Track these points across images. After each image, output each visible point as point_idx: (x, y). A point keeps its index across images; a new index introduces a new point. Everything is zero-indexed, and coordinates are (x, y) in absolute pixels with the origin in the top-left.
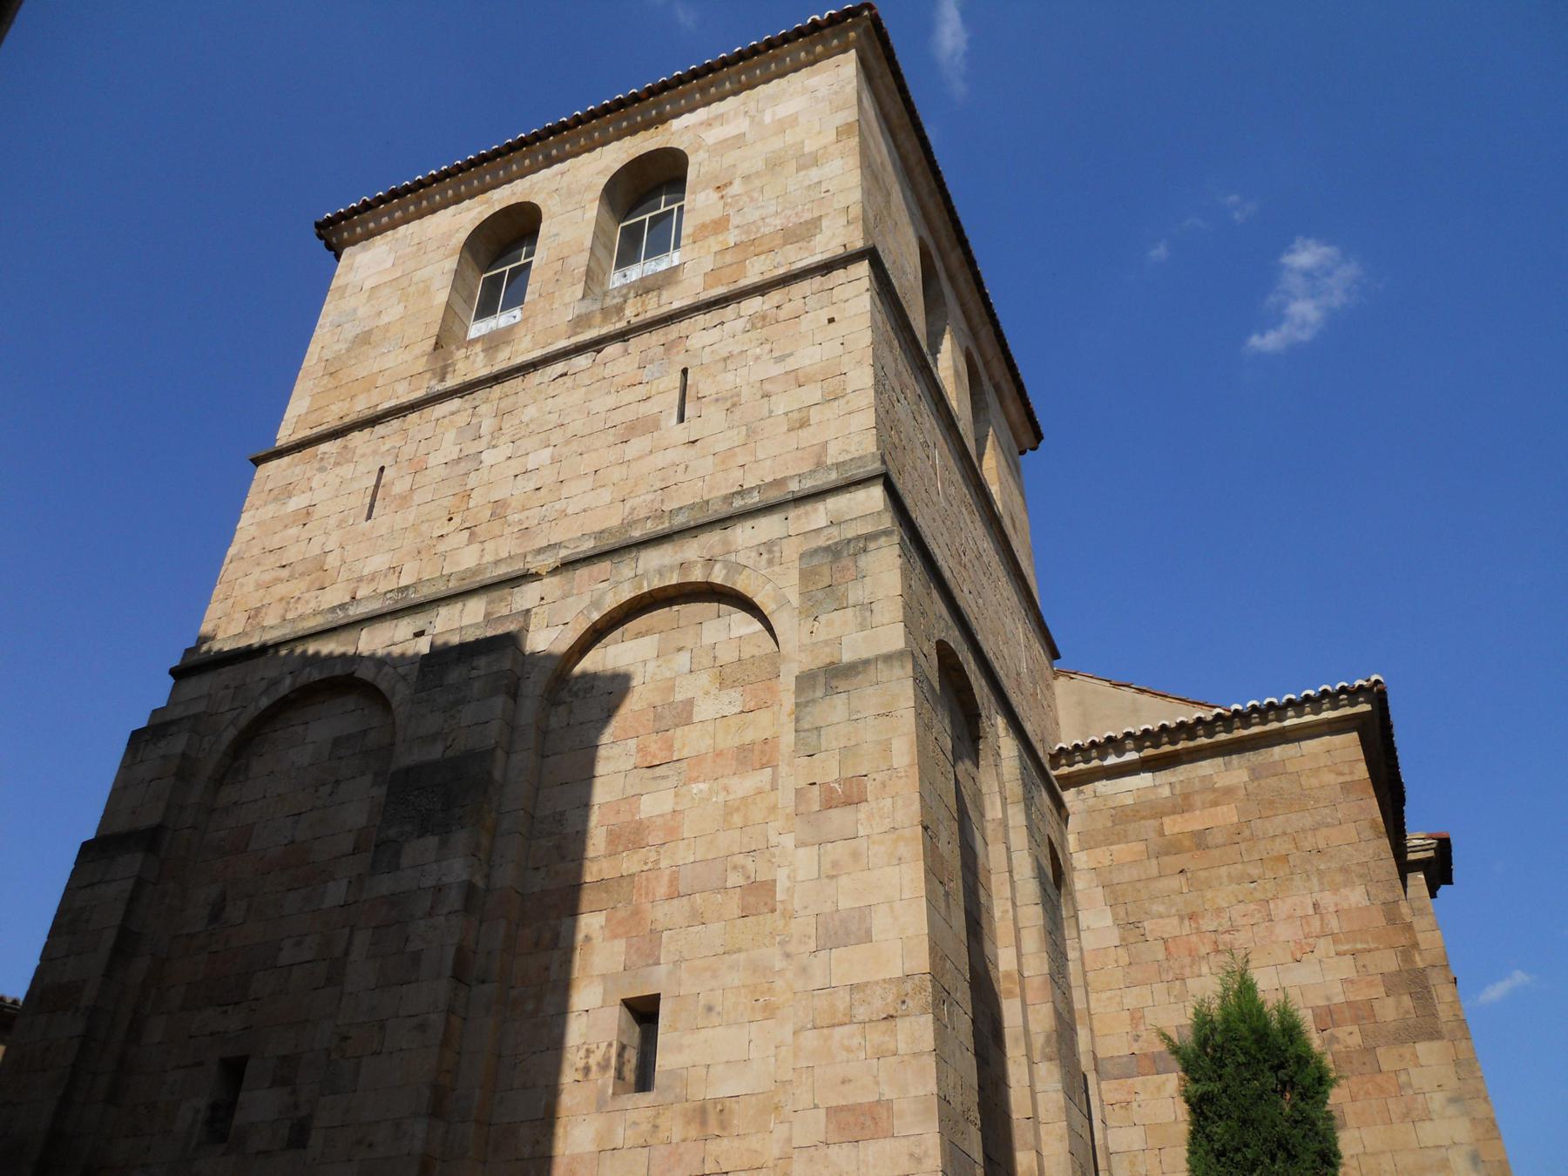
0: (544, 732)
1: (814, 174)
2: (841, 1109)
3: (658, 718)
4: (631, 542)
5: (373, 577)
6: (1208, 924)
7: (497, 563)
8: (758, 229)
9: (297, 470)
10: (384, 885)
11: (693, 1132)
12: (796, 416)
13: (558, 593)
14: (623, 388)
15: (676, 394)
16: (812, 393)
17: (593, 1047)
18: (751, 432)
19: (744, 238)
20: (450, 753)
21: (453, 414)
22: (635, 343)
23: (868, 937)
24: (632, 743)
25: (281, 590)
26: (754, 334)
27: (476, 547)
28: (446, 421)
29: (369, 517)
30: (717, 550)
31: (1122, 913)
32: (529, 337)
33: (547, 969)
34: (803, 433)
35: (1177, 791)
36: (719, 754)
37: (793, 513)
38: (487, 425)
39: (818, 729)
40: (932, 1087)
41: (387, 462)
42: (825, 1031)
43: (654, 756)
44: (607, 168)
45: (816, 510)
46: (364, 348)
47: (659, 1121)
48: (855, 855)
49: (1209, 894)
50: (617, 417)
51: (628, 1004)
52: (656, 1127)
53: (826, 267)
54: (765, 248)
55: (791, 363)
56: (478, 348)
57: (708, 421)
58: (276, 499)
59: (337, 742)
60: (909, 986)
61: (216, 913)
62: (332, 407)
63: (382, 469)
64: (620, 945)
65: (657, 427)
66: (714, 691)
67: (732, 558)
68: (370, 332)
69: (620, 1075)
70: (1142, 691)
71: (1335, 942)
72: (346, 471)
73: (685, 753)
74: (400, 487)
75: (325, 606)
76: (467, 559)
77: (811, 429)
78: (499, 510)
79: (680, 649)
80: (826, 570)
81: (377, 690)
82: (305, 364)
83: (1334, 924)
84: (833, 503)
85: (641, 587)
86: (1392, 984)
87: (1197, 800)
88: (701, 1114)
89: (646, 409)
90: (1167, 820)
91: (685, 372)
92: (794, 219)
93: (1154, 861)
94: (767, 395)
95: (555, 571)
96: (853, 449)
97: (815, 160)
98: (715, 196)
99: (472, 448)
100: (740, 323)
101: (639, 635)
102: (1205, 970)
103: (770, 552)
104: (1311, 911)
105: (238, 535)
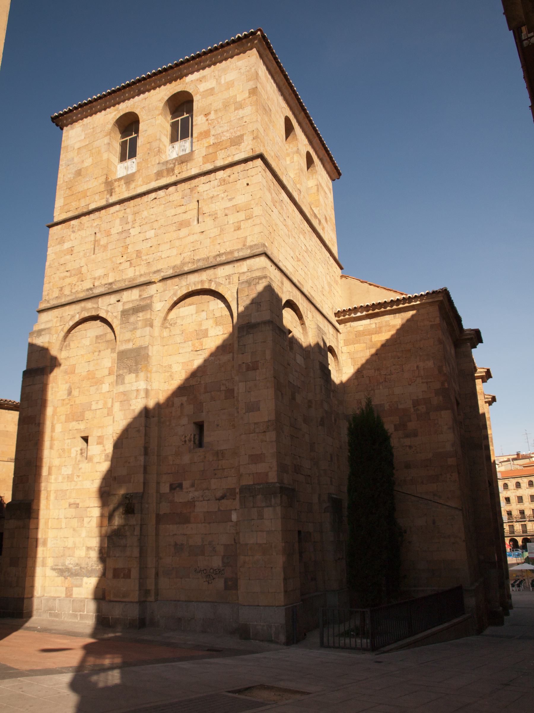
1: (241, 113)
2: (252, 455)
3: (197, 334)
4: (184, 272)
7: (141, 275)
8: (221, 137)
9: (65, 231)
10: (121, 388)
12: (236, 224)
13: (162, 289)
14: (177, 206)
15: (196, 211)
16: (241, 216)
18: (222, 230)
19: (216, 141)
20: (134, 347)
21: (117, 211)
23: (259, 409)
24: (190, 343)
25: (68, 280)
27: (132, 268)
28: (115, 215)
29: (94, 254)
30: (212, 277)
32: (141, 179)
35: (377, 326)
37: (236, 265)
39: (245, 345)
40: (275, 450)
41: (97, 230)
43: (197, 348)
46: (80, 177)
47: (243, 225)
50: (176, 219)
51: (195, 423)
53: (245, 161)
54: (224, 147)
56: (122, 182)
57: (208, 223)
58: (59, 243)
59: (97, 337)
62: (72, 204)
64: (192, 406)
66: (214, 326)
67: (217, 280)
68: (80, 170)
69: (195, 443)
70: (370, 285)
72: (83, 233)
74: (103, 242)
75: (84, 288)
76: (131, 274)
77: (241, 231)
78: (139, 254)
79: (203, 311)
80: (246, 289)
82: (58, 183)
84: (249, 262)
85: (189, 289)
87: (384, 329)
88: (217, 453)
90: (373, 336)
92: (234, 134)
95: (160, 281)
96: (255, 240)
97: (240, 106)
98: (205, 119)
99: (127, 227)
101: (190, 305)
102: (381, 387)
104: (415, 369)
105: (48, 257)
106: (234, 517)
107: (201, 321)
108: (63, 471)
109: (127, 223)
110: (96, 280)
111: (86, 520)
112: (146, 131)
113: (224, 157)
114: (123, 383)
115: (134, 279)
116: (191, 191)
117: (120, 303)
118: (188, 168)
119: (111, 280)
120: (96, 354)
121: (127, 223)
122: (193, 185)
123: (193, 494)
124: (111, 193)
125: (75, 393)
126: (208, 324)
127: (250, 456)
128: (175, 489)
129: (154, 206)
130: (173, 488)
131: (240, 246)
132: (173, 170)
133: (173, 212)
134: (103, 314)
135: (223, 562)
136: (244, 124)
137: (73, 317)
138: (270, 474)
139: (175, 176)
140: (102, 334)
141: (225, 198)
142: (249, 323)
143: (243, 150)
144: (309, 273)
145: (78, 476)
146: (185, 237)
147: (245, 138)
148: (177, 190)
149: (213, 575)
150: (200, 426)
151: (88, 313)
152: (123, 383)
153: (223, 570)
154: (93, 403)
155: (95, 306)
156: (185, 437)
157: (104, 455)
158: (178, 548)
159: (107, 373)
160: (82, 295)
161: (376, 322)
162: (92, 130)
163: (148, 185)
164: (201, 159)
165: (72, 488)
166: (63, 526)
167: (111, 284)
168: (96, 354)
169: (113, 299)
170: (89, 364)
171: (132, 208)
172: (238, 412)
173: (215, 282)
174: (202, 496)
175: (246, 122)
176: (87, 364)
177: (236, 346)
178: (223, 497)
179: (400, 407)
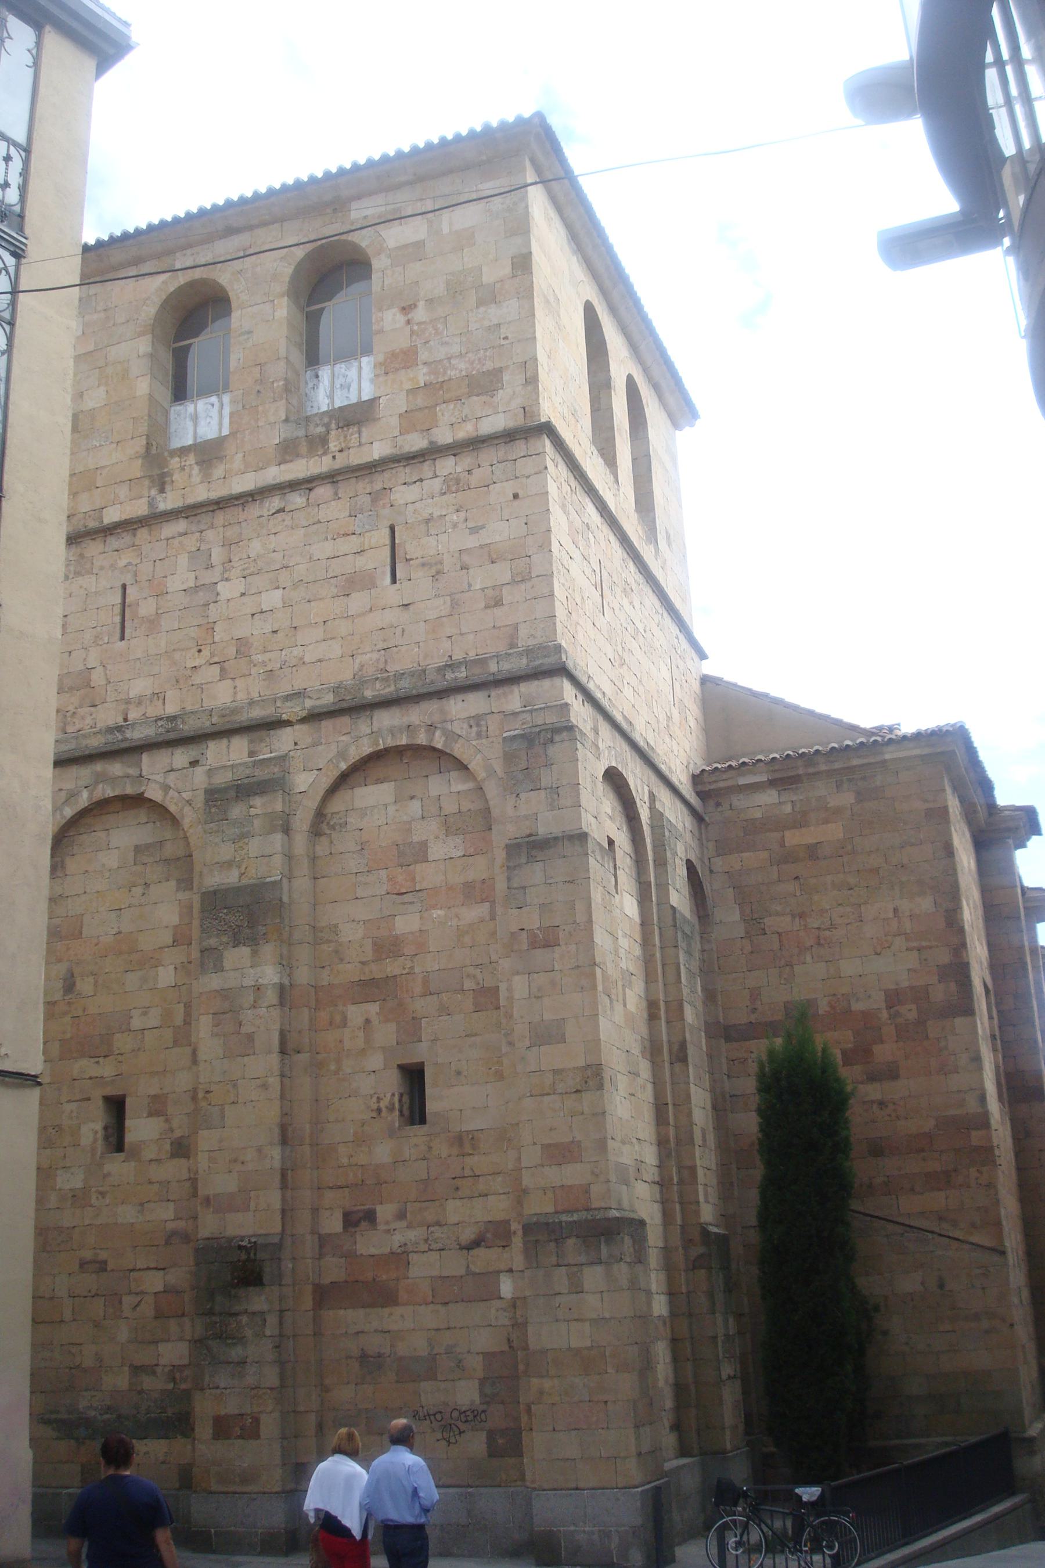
0: (314, 859)
2: (549, 1145)
6: (814, 923)
10: (213, 982)
12: (490, 593)
15: (387, 551)
16: (502, 573)
17: (382, 1096)
18: (455, 604)
20: (245, 881)
21: (181, 535)
22: (346, 489)
26: (450, 498)
28: (176, 541)
29: (122, 638)
30: (436, 718)
31: (748, 911)
34: (498, 612)
39: (524, 888)
41: (128, 579)
49: (816, 898)
51: (402, 1068)
52: (430, 1148)
55: (484, 537)
56: (191, 459)
57: (417, 585)
59: (138, 849)
60: (589, 1072)
63: (124, 587)
64: (392, 1027)
65: (374, 585)
71: (907, 940)
73: (424, 886)
74: (147, 608)
75: (100, 725)
76: (222, 696)
78: (242, 646)
79: (412, 798)
81: (166, 810)
83: (908, 926)
84: (525, 688)
85: (378, 745)
88: (459, 1140)
90: (787, 833)
93: (775, 868)
94: (464, 567)
95: (303, 720)
98: (401, 319)
99: (207, 577)
100: (437, 484)
102: (809, 959)
103: (478, 725)
104: (891, 915)
106: (507, 1287)
107: (410, 822)
108: (59, 1180)
109: (210, 566)
110: (131, 707)
111: (128, 1301)
112: (250, 332)
113: (454, 420)
114: (219, 968)
115: (235, 711)
116: (374, 501)
117: (199, 770)
118: (363, 440)
119: (171, 709)
120: (138, 891)
121: (210, 566)
122: (378, 486)
123: (402, 1236)
124: (161, 483)
125: (85, 986)
126: (427, 831)
127: (546, 1147)
128: (356, 1224)
129: (279, 528)
130: (351, 1221)
131: (502, 648)
132: (324, 440)
133: (328, 548)
134: (154, 793)
135: (482, 1394)
136: (503, 342)
137: (72, 795)
138: (594, 1189)
139: (330, 456)
140: (150, 840)
141: (462, 526)
142: (531, 835)
143: (500, 409)
144: (641, 687)
145: (103, 1194)
146: (363, 614)
147: (506, 377)
148: (336, 494)
149: (459, 1423)
150: (414, 1077)
151: (113, 789)
152: (219, 968)
153: (484, 1411)
154: (135, 1013)
155: (133, 771)
156: (379, 1099)
157: (169, 1141)
158: (370, 1363)
159: (170, 941)
160: (96, 743)
161: (794, 798)
162: (102, 315)
163: (260, 473)
164: (395, 421)
165: (87, 1222)
166: (67, 1315)
167: (172, 719)
168: (138, 891)
169: (180, 757)
170: (119, 916)
171: (221, 529)
172: (510, 1044)
173: (444, 729)
174: (426, 1241)
175: (506, 338)
176: (113, 914)
177: (501, 885)
178: (477, 1243)
179: (857, 1006)
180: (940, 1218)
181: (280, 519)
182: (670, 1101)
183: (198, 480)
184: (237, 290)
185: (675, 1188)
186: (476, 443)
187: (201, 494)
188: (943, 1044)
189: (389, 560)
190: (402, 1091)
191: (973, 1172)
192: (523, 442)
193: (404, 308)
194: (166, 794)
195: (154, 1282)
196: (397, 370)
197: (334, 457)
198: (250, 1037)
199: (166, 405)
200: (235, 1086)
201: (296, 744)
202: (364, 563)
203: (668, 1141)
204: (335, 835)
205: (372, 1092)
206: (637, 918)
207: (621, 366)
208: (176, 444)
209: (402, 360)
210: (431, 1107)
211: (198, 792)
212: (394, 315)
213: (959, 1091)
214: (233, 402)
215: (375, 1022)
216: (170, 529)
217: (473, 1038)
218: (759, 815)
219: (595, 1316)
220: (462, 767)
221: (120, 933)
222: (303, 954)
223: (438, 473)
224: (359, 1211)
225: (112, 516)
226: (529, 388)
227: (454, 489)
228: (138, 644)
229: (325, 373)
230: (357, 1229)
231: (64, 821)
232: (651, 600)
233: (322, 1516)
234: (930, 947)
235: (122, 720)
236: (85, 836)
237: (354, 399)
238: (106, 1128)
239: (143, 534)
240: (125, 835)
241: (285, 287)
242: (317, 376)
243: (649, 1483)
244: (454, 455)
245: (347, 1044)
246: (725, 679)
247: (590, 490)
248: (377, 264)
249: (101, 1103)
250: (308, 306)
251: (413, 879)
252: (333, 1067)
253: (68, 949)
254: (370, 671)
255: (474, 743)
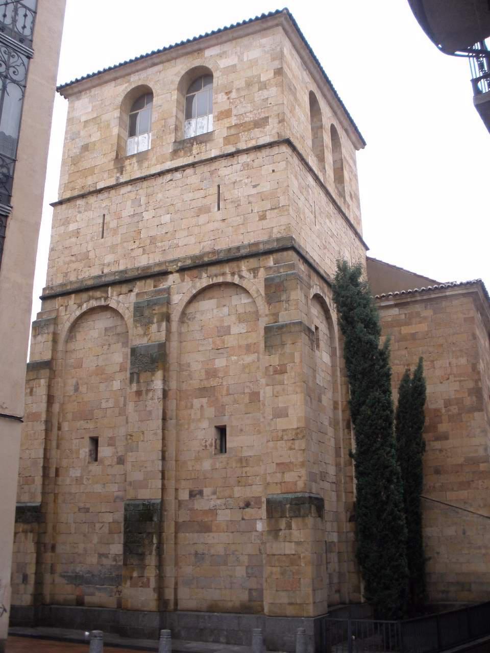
0: (180, 334)
3: (219, 331)
5: (109, 265)
11: (239, 465)
12: (261, 213)
21: (129, 192)
22: (200, 169)
23: (287, 416)
26: (245, 172)
27: (146, 256)
28: (126, 195)
29: (103, 237)
33: (190, 415)
34: (264, 222)
36: (240, 347)
38: (143, 200)
41: (106, 212)
42: (275, 442)
43: (219, 346)
44: (179, 72)
45: (269, 258)
48: (283, 390)
50: (194, 204)
51: (217, 427)
52: (228, 463)
55: (259, 189)
58: (63, 224)
59: (106, 329)
60: (298, 431)
61: (77, 389)
63: (104, 215)
64: (213, 409)
69: (216, 448)
71: (455, 377)
72: (90, 214)
74: (113, 224)
76: (143, 261)
77: (268, 220)
78: (153, 240)
79: (224, 306)
81: (118, 312)
83: (455, 370)
85: (210, 282)
86: (471, 392)
88: (241, 460)
89: (205, 201)
90: (402, 328)
91: (219, 186)
93: (397, 344)
99: (139, 210)
104: (448, 365)
108: (71, 473)
110: (104, 267)
111: (98, 526)
119: (122, 268)
120: (106, 347)
122: (213, 168)
123: (214, 502)
124: (121, 170)
125: (83, 389)
128: (195, 496)
130: (192, 495)
133: (191, 196)
134: (113, 304)
135: (247, 573)
139: (193, 156)
145: (88, 479)
148: (195, 172)
150: (222, 431)
154: (103, 401)
156: (206, 441)
157: (115, 457)
158: (199, 557)
160: (90, 283)
161: (406, 312)
162: (100, 102)
164: (221, 140)
165: (82, 491)
168: (106, 347)
170: (98, 359)
171: (145, 189)
172: (264, 417)
174: (225, 504)
175: (270, 104)
176: (95, 358)
180: (465, 503)
181: (170, 184)
182: (342, 447)
183: (137, 168)
184: (156, 89)
185: (343, 485)
186: (258, 148)
187: (138, 175)
188: (469, 424)
189: (217, 200)
190: (216, 438)
191: (480, 482)
192: (277, 147)
193: (226, 93)
194: (118, 304)
195: (109, 518)
196: (223, 119)
197: (195, 157)
198: (150, 412)
199: (126, 139)
200: (143, 433)
201: (174, 282)
202: (207, 201)
203: (340, 465)
204: (190, 323)
205: (203, 438)
206: (330, 364)
207: (327, 117)
208: (129, 154)
209: (225, 114)
210: (229, 445)
211: (131, 304)
212: (222, 95)
213: (476, 446)
214: (153, 135)
215: (205, 405)
216: (124, 190)
217: (248, 415)
218: (390, 320)
219: (297, 540)
220: (246, 291)
221: (98, 366)
222: (173, 374)
223: (239, 162)
224: (196, 490)
225: (100, 186)
226: (280, 124)
227: (246, 168)
228: (109, 240)
229: (193, 122)
230: (195, 498)
231: (76, 317)
232: (341, 221)
233: (22, 527)
234: (465, 380)
235: (101, 273)
236: (85, 324)
237: (205, 132)
238: (90, 451)
239: (113, 192)
240: (101, 323)
241: (176, 86)
242: (190, 123)
243: (319, 616)
244: (247, 154)
245: (193, 416)
246: (377, 259)
247: (310, 170)
248: (216, 75)
249: (88, 439)
250: (187, 93)
251: (224, 342)
252: (186, 427)
253: (76, 373)
254: (207, 250)
255: (252, 281)
